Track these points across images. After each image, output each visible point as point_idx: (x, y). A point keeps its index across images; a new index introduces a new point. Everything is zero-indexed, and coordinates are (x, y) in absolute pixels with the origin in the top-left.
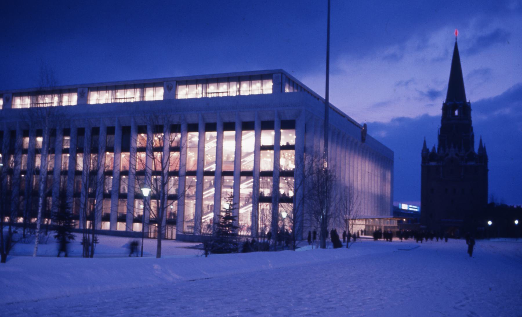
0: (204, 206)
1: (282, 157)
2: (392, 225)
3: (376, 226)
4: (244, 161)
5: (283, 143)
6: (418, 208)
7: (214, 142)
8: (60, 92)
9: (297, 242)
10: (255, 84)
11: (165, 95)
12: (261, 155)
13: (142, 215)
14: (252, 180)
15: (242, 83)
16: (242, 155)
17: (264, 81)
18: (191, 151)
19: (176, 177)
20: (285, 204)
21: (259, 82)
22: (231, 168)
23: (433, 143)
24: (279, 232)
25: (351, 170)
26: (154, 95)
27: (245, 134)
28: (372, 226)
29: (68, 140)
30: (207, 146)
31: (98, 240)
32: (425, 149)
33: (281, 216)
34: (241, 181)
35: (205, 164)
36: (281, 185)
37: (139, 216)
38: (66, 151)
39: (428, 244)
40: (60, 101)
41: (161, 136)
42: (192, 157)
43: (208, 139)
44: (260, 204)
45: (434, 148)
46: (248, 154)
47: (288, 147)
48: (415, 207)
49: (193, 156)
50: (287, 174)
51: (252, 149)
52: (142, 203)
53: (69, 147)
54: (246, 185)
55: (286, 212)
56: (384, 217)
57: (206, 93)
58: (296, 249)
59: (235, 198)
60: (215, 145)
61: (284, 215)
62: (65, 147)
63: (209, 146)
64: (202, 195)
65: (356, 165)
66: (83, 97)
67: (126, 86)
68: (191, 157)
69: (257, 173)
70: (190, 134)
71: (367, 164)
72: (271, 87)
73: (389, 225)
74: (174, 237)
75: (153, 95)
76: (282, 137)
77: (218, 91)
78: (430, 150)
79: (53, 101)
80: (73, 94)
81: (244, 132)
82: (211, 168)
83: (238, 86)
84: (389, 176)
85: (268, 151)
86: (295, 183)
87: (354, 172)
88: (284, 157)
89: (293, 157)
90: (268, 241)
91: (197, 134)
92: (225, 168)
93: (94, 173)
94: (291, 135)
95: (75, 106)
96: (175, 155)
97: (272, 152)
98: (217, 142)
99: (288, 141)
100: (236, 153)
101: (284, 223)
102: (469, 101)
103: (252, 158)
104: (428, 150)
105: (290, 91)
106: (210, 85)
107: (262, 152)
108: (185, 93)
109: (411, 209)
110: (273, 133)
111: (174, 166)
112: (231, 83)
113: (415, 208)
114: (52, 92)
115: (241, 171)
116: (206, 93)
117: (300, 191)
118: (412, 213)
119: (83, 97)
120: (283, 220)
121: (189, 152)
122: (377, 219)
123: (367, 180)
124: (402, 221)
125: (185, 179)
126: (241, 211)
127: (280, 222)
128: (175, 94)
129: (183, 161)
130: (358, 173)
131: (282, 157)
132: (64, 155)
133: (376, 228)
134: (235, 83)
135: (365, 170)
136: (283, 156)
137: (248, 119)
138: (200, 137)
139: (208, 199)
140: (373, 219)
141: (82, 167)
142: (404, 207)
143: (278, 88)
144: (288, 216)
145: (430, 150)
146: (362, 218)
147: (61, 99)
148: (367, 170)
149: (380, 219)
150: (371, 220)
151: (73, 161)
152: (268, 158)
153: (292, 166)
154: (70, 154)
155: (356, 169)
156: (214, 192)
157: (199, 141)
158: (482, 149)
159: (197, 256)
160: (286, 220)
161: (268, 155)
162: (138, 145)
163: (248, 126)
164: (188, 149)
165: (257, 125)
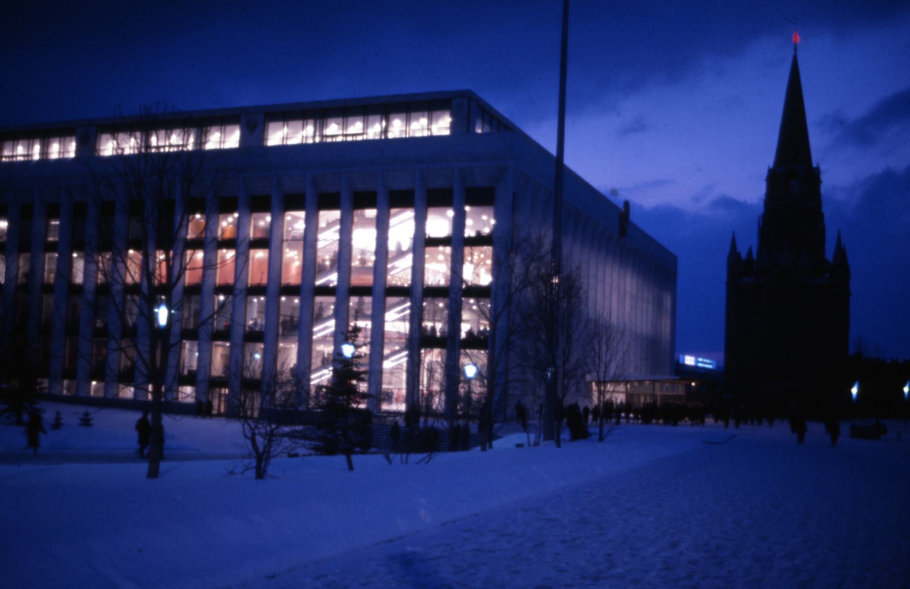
0: (314, 354)
1: (467, 261)
2: (675, 393)
3: (645, 396)
4: (393, 268)
5: (469, 232)
6: (714, 362)
7: (336, 232)
8: (45, 136)
9: (496, 426)
10: (417, 119)
11: (242, 140)
12: (427, 256)
13: (195, 371)
14: (408, 304)
15: (391, 116)
16: (390, 256)
17: (435, 114)
18: (292, 248)
19: (262, 298)
20: (475, 352)
21: (423, 116)
22: (368, 279)
23: (749, 243)
24: (827, 276)
25: (599, 288)
26: (222, 140)
27: (396, 214)
28: (639, 396)
29: (55, 225)
30: (324, 238)
31: (91, 419)
32: (734, 253)
33: (464, 373)
34: (387, 305)
35: (317, 270)
36: (465, 315)
37: (190, 372)
38: (52, 247)
39: (748, 431)
40: (44, 152)
41: (234, 218)
42: (293, 258)
43: (322, 224)
44: (423, 351)
45: (750, 253)
46: (400, 254)
47: (479, 240)
48: (708, 361)
49: (296, 257)
50: (477, 292)
51: (406, 244)
52: (196, 348)
53: (56, 239)
54: (397, 314)
55: (475, 364)
56: (658, 377)
57: (322, 136)
58: (494, 440)
59: (378, 337)
60: (337, 237)
61: (470, 371)
62: (51, 239)
63: (328, 239)
64: (311, 333)
65: (608, 280)
66: (88, 145)
67: (168, 124)
68: (292, 260)
69: (418, 291)
70: (289, 216)
71: (628, 278)
72: (448, 125)
73: (670, 393)
74: (256, 414)
75: (219, 140)
76: (469, 222)
77: (345, 133)
78: (744, 255)
79: (30, 153)
80: (68, 139)
81: (393, 211)
82: (330, 281)
83: (384, 124)
84: (668, 302)
85: (441, 248)
86: (494, 310)
87: (604, 291)
88: (471, 262)
89: (489, 262)
90: (434, 423)
91: (302, 214)
92: (357, 280)
93: (103, 290)
94: (484, 217)
95: (73, 160)
96: (260, 255)
97: (448, 250)
98: (341, 232)
99: (478, 229)
100: (377, 253)
101: (469, 387)
102: (818, 164)
103: (407, 262)
104: (739, 255)
105: (484, 131)
106: (329, 120)
107: (429, 250)
108: (282, 136)
109: (700, 365)
110: (450, 213)
111: (256, 274)
112: (371, 118)
113: (706, 364)
114: (28, 135)
115: (387, 286)
116: (322, 136)
117: (501, 323)
118: (703, 371)
119: (88, 145)
120: (468, 381)
121: (287, 250)
122: (647, 382)
123: (628, 309)
124: (690, 385)
125: (279, 301)
126: (387, 365)
127: (461, 385)
128: (263, 137)
129: (275, 264)
130: (611, 293)
131: (467, 261)
132: (47, 255)
133: (645, 399)
134: (378, 117)
135: (625, 289)
136: (469, 258)
137: (401, 184)
138: (308, 220)
139: (323, 340)
140: (641, 382)
141: (433, 354)
142: (689, 360)
143: (459, 126)
144: (479, 374)
145: (744, 255)
146: (621, 379)
147: (45, 149)
148: (628, 289)
149: (653, 382)
150: (636, 384)
151: (66, 266)
152: (440, 262)
153: (485, 279)
154: (59, 254)
155: (607, 287)
156: (332, 329)
157: (306, 230)
158: (840, 252)
159: (232, 472)
160: (473, 382)
161: (441, 257)
162: (190, 236)
163: (402, 200)
164: (285, 244)
165: (419, 196)
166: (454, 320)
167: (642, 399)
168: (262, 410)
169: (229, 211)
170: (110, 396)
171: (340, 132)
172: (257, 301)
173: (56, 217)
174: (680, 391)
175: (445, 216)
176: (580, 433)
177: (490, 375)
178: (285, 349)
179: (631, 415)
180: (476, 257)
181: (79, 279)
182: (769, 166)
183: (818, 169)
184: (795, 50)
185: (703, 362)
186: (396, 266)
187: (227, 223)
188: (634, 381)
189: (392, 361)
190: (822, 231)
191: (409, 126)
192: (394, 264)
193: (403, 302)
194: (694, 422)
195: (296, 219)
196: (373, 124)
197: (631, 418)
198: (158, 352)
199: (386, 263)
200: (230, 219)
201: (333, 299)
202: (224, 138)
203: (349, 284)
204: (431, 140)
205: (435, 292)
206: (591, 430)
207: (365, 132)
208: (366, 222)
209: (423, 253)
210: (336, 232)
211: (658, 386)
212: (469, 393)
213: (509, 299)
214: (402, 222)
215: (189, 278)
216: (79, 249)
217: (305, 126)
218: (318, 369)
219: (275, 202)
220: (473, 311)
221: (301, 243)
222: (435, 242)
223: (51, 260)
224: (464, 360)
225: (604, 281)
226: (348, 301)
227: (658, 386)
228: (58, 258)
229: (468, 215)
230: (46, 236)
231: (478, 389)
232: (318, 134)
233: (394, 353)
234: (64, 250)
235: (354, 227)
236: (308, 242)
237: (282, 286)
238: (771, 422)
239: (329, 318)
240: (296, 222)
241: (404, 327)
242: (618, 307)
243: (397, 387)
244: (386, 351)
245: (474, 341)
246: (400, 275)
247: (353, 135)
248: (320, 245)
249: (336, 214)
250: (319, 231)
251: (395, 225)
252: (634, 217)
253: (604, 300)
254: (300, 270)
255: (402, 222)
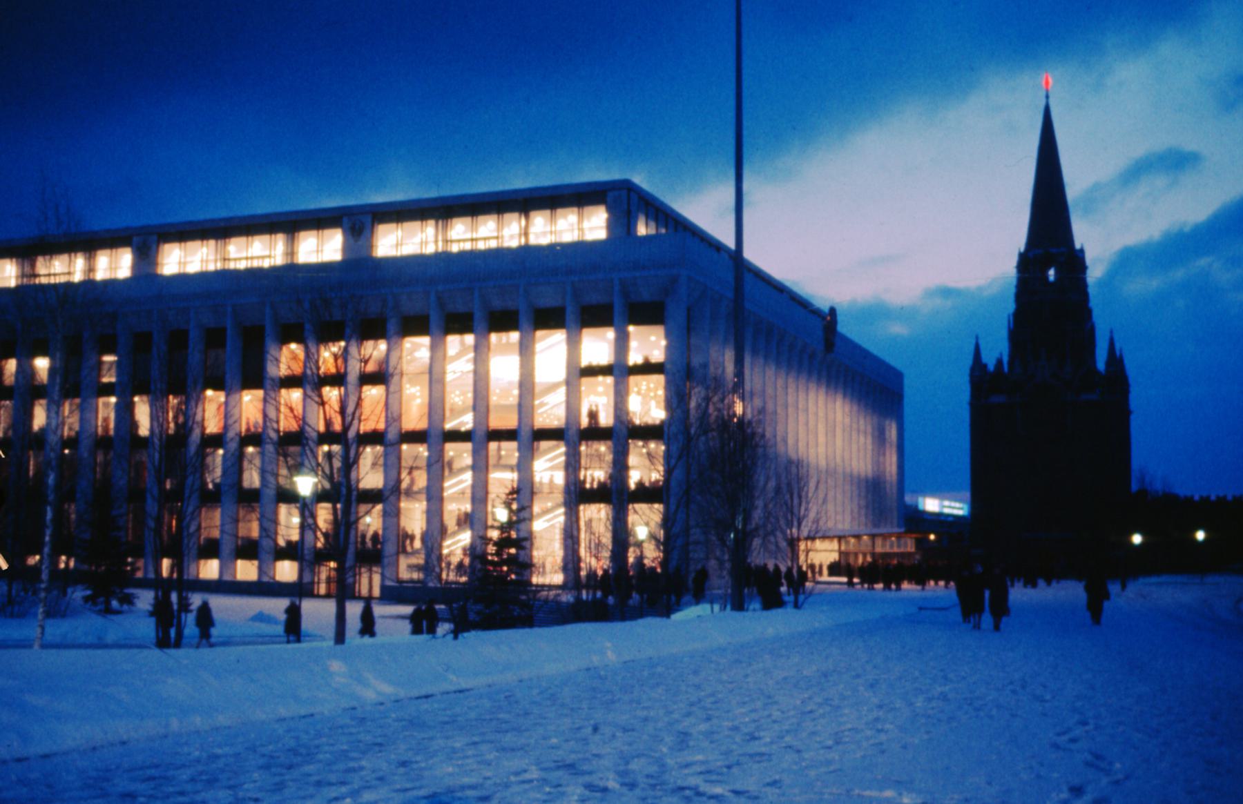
2: (902, 550)
3: (865, 555)
4: (542, 405)
5: (635, 358)
8: (90, 244)
11: (346, 248)
12: (583, 388)
13: (297, 543)
18: (413, 384)
22: (511, 422)
23: (996, 349)
26: (320, 249)
27: (543, 338)
28: (856, 555)
32: (978, 363)
33: (635, 536)
38: (108, 390)
45: (999, 362)
46: (553, 387)
47: (647, 368)
48: (958, 505)
50: (647, 433)
51: (560, 374)
53: (113, 380)
56: (876, 531)
57: (446, 241)
60: (470, 367)
61: (641, 532)
62: (105, 380)
68: (413, 397)
70: (409, 342)
71: (839, 403)
73: (896, 550)
75: (315, 249)
76: (633, 344)
78: (991, 367)
81: (539, 333)
82: (462, 424)
84: (892, 432)
85: (600, 378)
87: (807, 424)
88: (639, 393)
89: (661, 392)
91: (425, 340)
92: (496, 422)
94: (653, 338)
96: (373, 393)
97: (609, 380)
101: (642, 552)
103: (560, 395)
104: (985, 366)
107: (586, 382)
109: (946, 511)
113: (957, 508)
116: (446, 241)
117: (678, 474)
118: (951, 519)
120: (639, 545)
121: (408, 386)
122: (865, 537)
123: (839, 443)
126: (538, 526)
127: (631, 549)
132: (101, 400)
134: (516, 215)
138: (433, 348)
140: (858, 537)
144: (652, 536)
145: (991, 367)
146: (831, 534)
149: (873, 537)
150: (852, 540)
151: (125, 412)
152: (600, 394)
153: (657, 414)
158: (1115, 361)
160: (645, 545)
162: (283, 371)
163: (549, 319)
166: (620, 466)
167: (860, 560)
168: (383, 588)
169: (335, 338)
170: (227, 578)
171: (468, 236)
172: (370, 453)
173: (109, 352)
174: (909, 546)
175: (604, 339)
176: (772, 601)
177: (670, 537)
178: (409, 509)
179: (856, 580)
180: (644, 387)
181: (144, 431)
182: (1019, 249)
183: (1082, 251)
184: (1047, 97)
185: (950, 507)
186: (545, 401)
187: (327, 356)
188: (849, 536)
189: (545, 521)
190: (1092, 331)
191: (555, 224)
192: (542, 399)
193: (558, 447)
194: (871, 586)
195: (416, 347)
196: (510, 223)
197: (857, 584)
198: (342, 536)
199: (533, 399)
200: (335, 349)
201: (468, 446)
202: (322, 246)
203: (488, 427)
204: (580, 249)
205: (594, 433)
206: (786, 598)
207: (500, 234)
208: (504, 349)
209: (579, 385)
210: (468, 361)
211: (879, 542)
212: (640, 559)
213: (689, 439)
214: (549, 347)
215: (287, 424)
216: (141, 391)
217: (424, 228)
218: (454, 534)
219: (392, 325)
220: (642, 455)
221: (426, 377)
222: (591, 371)
223: (107, 407)
224: (632, 518)
225: (807, 410)
226: (487, 449)
227: (879, 542)
228: (117, 404)
229: (632, 337)
230: (99, 376)
231: (652, 555)
232: (440, 238)
233: (546, 512)
234: (126, 390)
235: (491, 354)
236: (435, 377)
237: (403, 431)
238: (1049, 583)
239: (462, 470)
240: (417, 349)
241: (559, 478)
242: (827, 443)
243: (1047, 705)
244: (536, 509)
245: (646, 494)
246: (549, 412)
247: (485, 239)
248: (449, 377)
249: (470, 339)
250: (448, 360)
251: (542, 351)
252: (843, 328)
253: (808, 435)
254: (426, 410)
255: (549, 347)
